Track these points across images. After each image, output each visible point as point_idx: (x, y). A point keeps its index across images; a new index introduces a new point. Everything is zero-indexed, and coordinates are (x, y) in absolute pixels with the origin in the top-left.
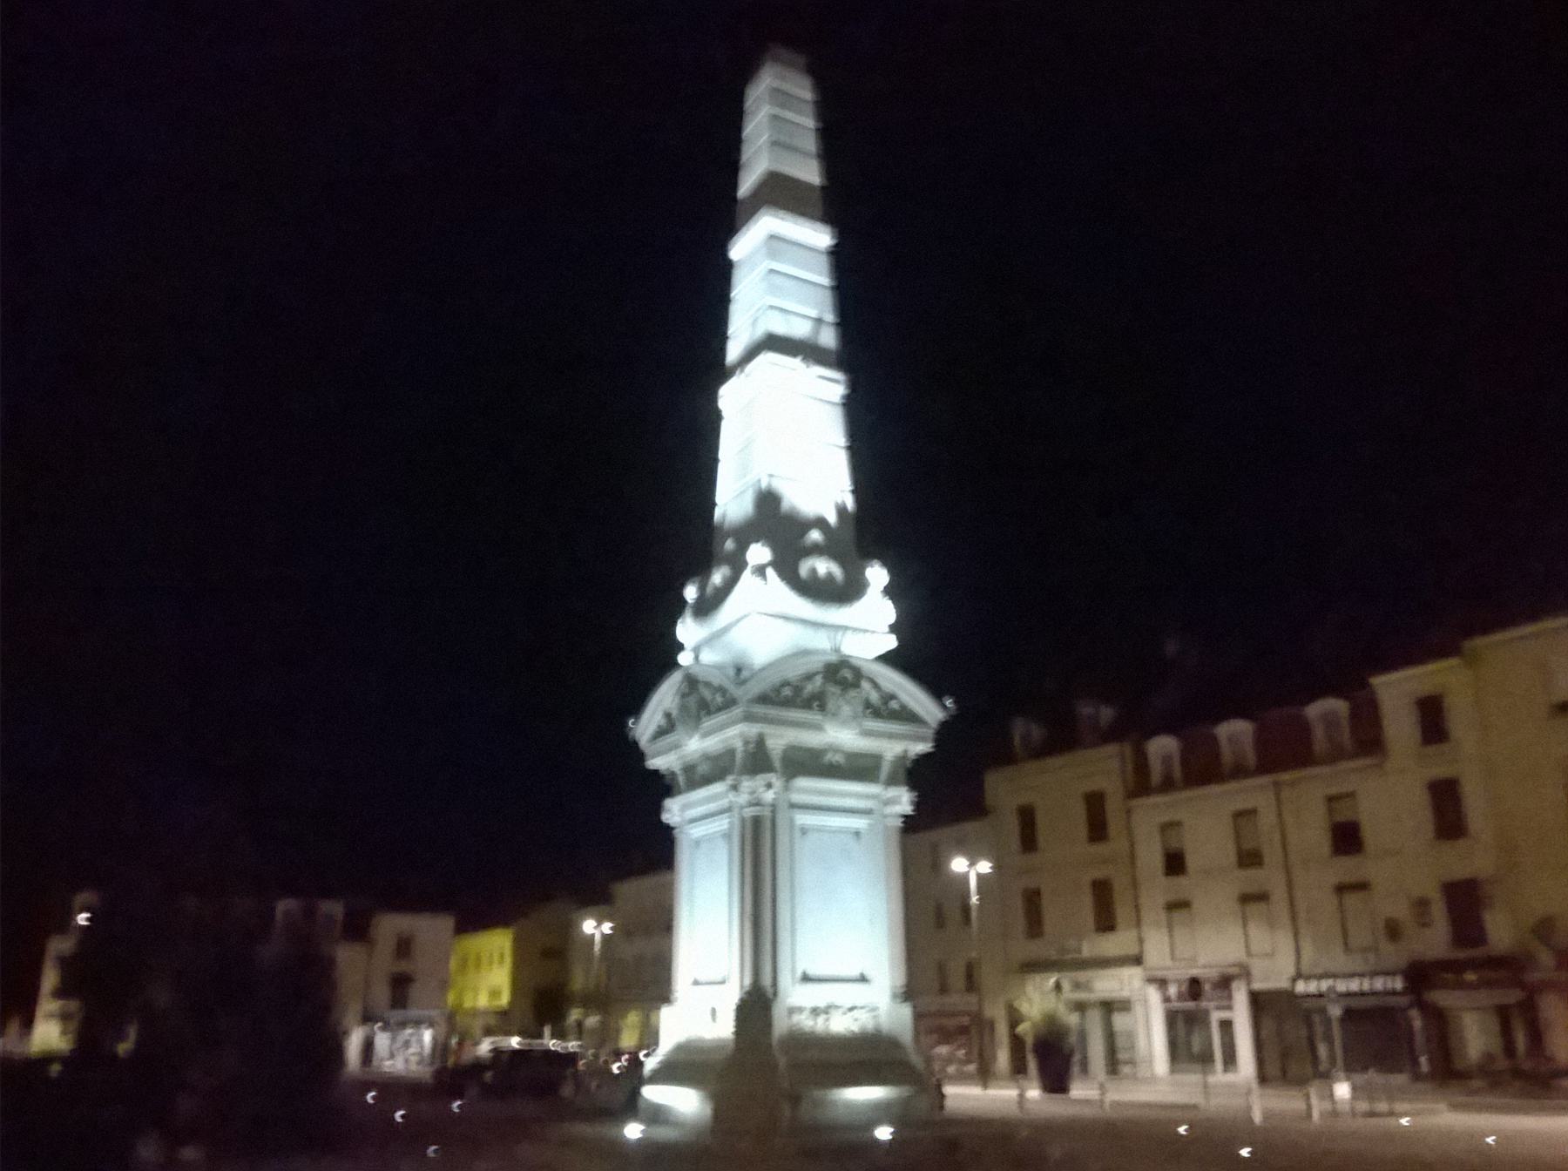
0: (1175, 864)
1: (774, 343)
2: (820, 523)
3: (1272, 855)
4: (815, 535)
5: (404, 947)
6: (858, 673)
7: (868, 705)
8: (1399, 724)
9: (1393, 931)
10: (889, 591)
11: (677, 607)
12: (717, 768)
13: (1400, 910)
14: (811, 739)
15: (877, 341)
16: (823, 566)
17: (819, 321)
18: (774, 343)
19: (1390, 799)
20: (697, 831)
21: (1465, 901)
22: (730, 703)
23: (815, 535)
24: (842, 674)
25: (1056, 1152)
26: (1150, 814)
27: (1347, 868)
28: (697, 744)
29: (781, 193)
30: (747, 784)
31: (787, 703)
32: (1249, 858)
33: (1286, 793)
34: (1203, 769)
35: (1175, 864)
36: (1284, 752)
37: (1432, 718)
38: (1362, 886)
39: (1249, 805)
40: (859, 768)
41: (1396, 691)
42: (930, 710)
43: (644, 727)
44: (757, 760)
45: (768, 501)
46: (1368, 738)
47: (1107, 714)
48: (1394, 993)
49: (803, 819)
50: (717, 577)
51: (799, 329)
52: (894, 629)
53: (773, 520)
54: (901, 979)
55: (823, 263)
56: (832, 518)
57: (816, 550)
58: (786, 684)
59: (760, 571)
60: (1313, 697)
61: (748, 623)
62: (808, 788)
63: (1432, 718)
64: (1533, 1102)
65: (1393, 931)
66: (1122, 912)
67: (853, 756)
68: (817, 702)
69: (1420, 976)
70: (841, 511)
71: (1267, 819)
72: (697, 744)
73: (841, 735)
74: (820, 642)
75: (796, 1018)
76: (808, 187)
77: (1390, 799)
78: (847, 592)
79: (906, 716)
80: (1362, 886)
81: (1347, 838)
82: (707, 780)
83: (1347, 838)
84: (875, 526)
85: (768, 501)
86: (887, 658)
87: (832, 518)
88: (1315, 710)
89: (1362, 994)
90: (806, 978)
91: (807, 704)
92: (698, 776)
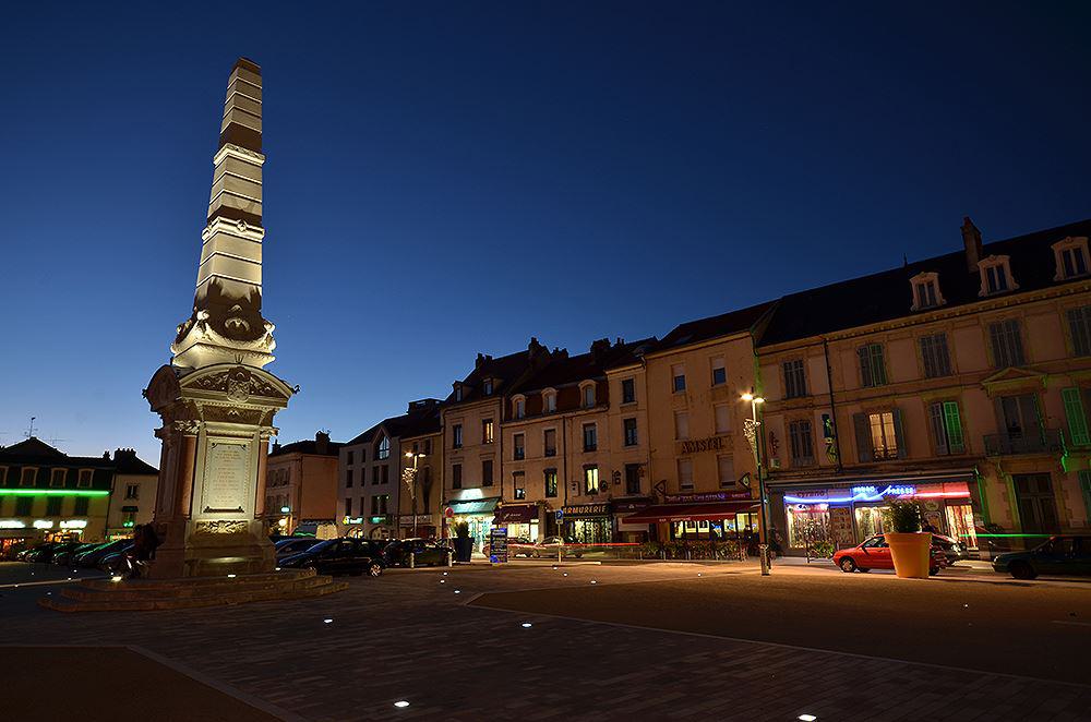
0: (519, 456)
1: (226, 212)
7: (252, 388)
8: (616, 393)
18: (226, 212)
19: (608, 427)
21: (633, 472)
25: (35, 500)
26: (511, 432)
29: (239, 137)
31: (206, 387)
32: (550, 452)
34: (535, 410)
35: (519, 456)
37: (628, 388)
45: (214, 288)
46: (603, 399)
49: (212, 440)
54: (259, 511)
57: (237, 314)
58: (207, 378)
59: (202, 325)
62: (214, 426)
63: (628, 388)
64: (843, 584)
66: (496, 479)
68: (225, 387)
71: (559, 434)
75: (201, 528)
77: (608, 427)
85: (214, 288)
90: (208, 510)
91: (218, 389)
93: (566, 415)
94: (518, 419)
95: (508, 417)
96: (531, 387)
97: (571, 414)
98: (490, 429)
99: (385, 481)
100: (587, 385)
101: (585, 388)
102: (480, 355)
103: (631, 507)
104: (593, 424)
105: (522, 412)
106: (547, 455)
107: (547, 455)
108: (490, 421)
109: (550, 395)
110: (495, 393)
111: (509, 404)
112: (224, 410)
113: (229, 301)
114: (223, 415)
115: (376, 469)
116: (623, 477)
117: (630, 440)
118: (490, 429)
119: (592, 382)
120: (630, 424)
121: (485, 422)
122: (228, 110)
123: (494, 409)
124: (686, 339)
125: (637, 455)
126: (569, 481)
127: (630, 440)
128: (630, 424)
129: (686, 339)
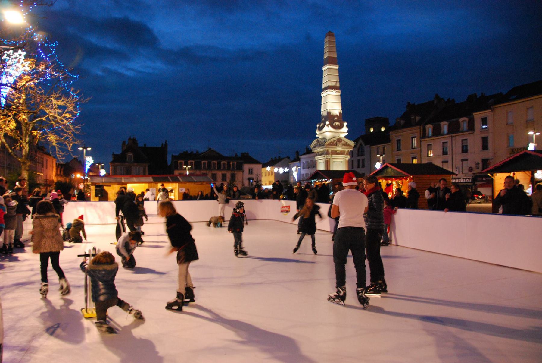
2: (337, 116)
3: (449, 152)
4: (336, 118)
5: (251, 171)
6: (342, 140)
9: (471, 169)
10: (347, 126)
11: (316, 128)
12: (322, 154)
13: (473, 166)
14: (335, 149)
15: (345, 89)
16: (337, 123)
17: (337, 82)
19: (474, 141)
20: (320, 161)
22: (323, 145)
23: (336, 118)
24: (339, 140)
27: (464, 156)
28: (319, 150)
29: (331, 61)
30: (326, 156)
31: (331, 145)
33: (454, 138)
34: (437, 132)
36: (454, 129)
38: (467, 160)
39: (446, 141)
40: (342, 153)
41: (478, 116)
42: (352, 143)
43: (312, 145)
44: (327, 153)
46: (471, 127)
47: (418, 118)
48: (469, 182)
50: (322, 125)
51: (333, 84)
52: (347, 132)
53: (330, 117)
55: (337, 71)
56: (338, 115)
59: (328, 125)
60: (461, 117)
61: (327, 132)
62: (335, 156)
65: (471, 169)
67: (341, 151)
68: (336, 144)
69: (475, 179)
70: (340, 113)
71: (449, 144)
72: (319, 150)
73: (339, 149)
74: (336, 135)
76: (335, 58)
77: (474, 141)
78: (341, 127)
79: (349, 145)
80: (467, 160)
81: (465, 150)
82: (321, 155)
83: (465, 150)
84: (345, 115)
85: (329, 113)
86: (346, 137)
87: (338, 115)
88: (461, 120)
89: (463, 183)
91: (334, 145)
92: (319, 154)
93: (453, 135)
94: (428, 137)
95: (424, 135)
96: (436, 121)
97: (455, 135)
98: (415, 142)
99: (363, 166)
100: (464, 122)
101: (463, 121)
102: (408, 103)
103: (484, 179)
104: (466, 140)
105: (431, 133)
106: (443, 154)
107: (443, 154)
108: (415, 137)
109: (445, 126)
110: (419, 123)
111: (424, 131)
112: (336, 151)
113: (333, 117)
114: (336, 153)
115: (359, 161)
116: (481, 165)
117: (485, 147)
118: (415, 142)
119: (465, 118)
120: (485, 141)
121: (412, 138)
122: (326, 50)
123: (416, 130)
124: (514, 97)
125: (488, 154)
126: (454, 166)
127: (485, 147)
128: (485, 141)
129: (514, 97)
